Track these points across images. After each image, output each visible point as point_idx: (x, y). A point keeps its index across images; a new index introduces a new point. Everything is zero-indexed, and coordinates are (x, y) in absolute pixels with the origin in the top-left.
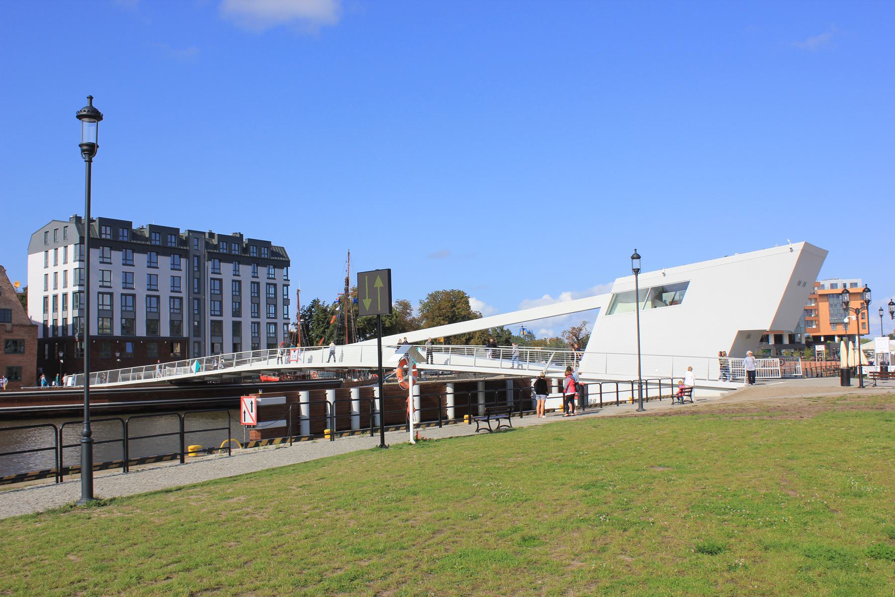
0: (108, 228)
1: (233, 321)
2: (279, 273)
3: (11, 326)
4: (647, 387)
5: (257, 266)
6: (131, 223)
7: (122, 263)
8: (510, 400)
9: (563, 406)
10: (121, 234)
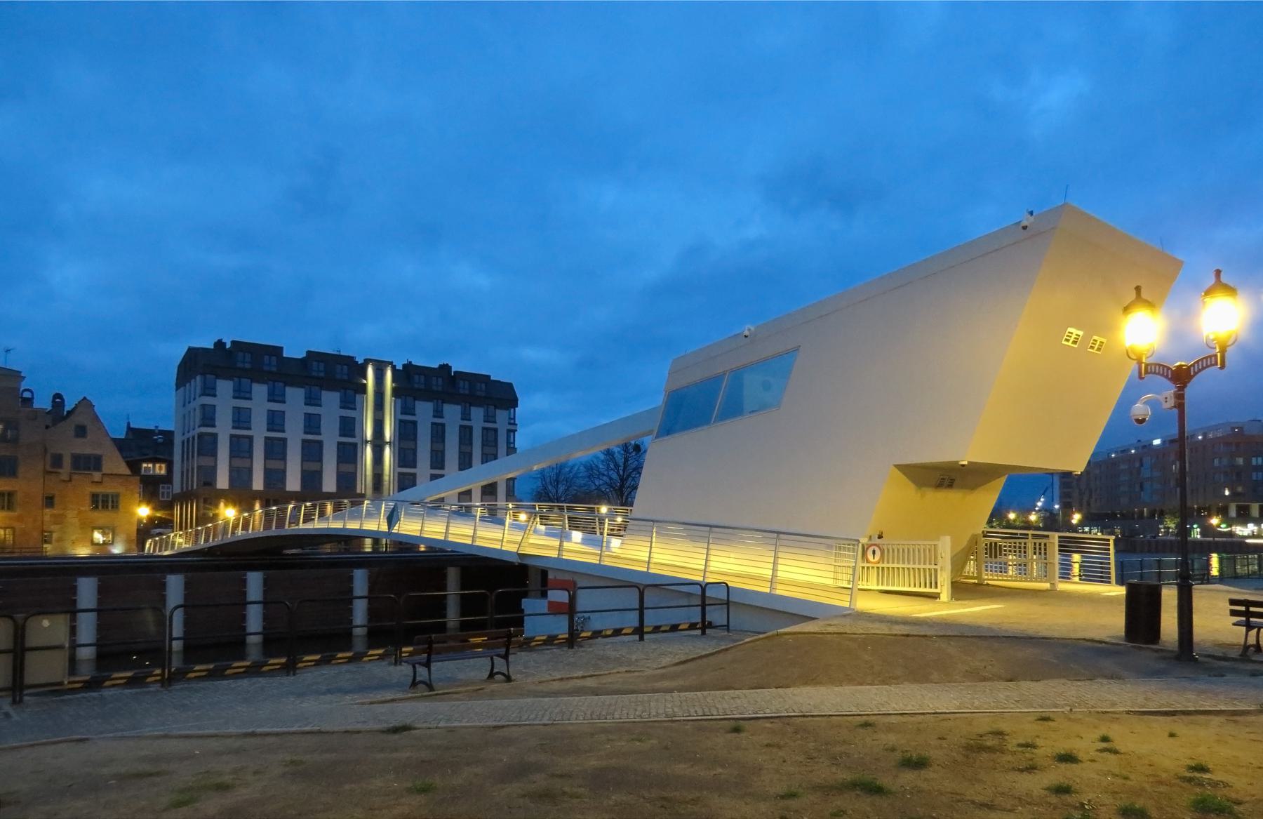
2: (501, 415)
4: (447, 529)
5: (443, 402)
7: (232, 395)
9: (1229, 656)
10: (434, 382)
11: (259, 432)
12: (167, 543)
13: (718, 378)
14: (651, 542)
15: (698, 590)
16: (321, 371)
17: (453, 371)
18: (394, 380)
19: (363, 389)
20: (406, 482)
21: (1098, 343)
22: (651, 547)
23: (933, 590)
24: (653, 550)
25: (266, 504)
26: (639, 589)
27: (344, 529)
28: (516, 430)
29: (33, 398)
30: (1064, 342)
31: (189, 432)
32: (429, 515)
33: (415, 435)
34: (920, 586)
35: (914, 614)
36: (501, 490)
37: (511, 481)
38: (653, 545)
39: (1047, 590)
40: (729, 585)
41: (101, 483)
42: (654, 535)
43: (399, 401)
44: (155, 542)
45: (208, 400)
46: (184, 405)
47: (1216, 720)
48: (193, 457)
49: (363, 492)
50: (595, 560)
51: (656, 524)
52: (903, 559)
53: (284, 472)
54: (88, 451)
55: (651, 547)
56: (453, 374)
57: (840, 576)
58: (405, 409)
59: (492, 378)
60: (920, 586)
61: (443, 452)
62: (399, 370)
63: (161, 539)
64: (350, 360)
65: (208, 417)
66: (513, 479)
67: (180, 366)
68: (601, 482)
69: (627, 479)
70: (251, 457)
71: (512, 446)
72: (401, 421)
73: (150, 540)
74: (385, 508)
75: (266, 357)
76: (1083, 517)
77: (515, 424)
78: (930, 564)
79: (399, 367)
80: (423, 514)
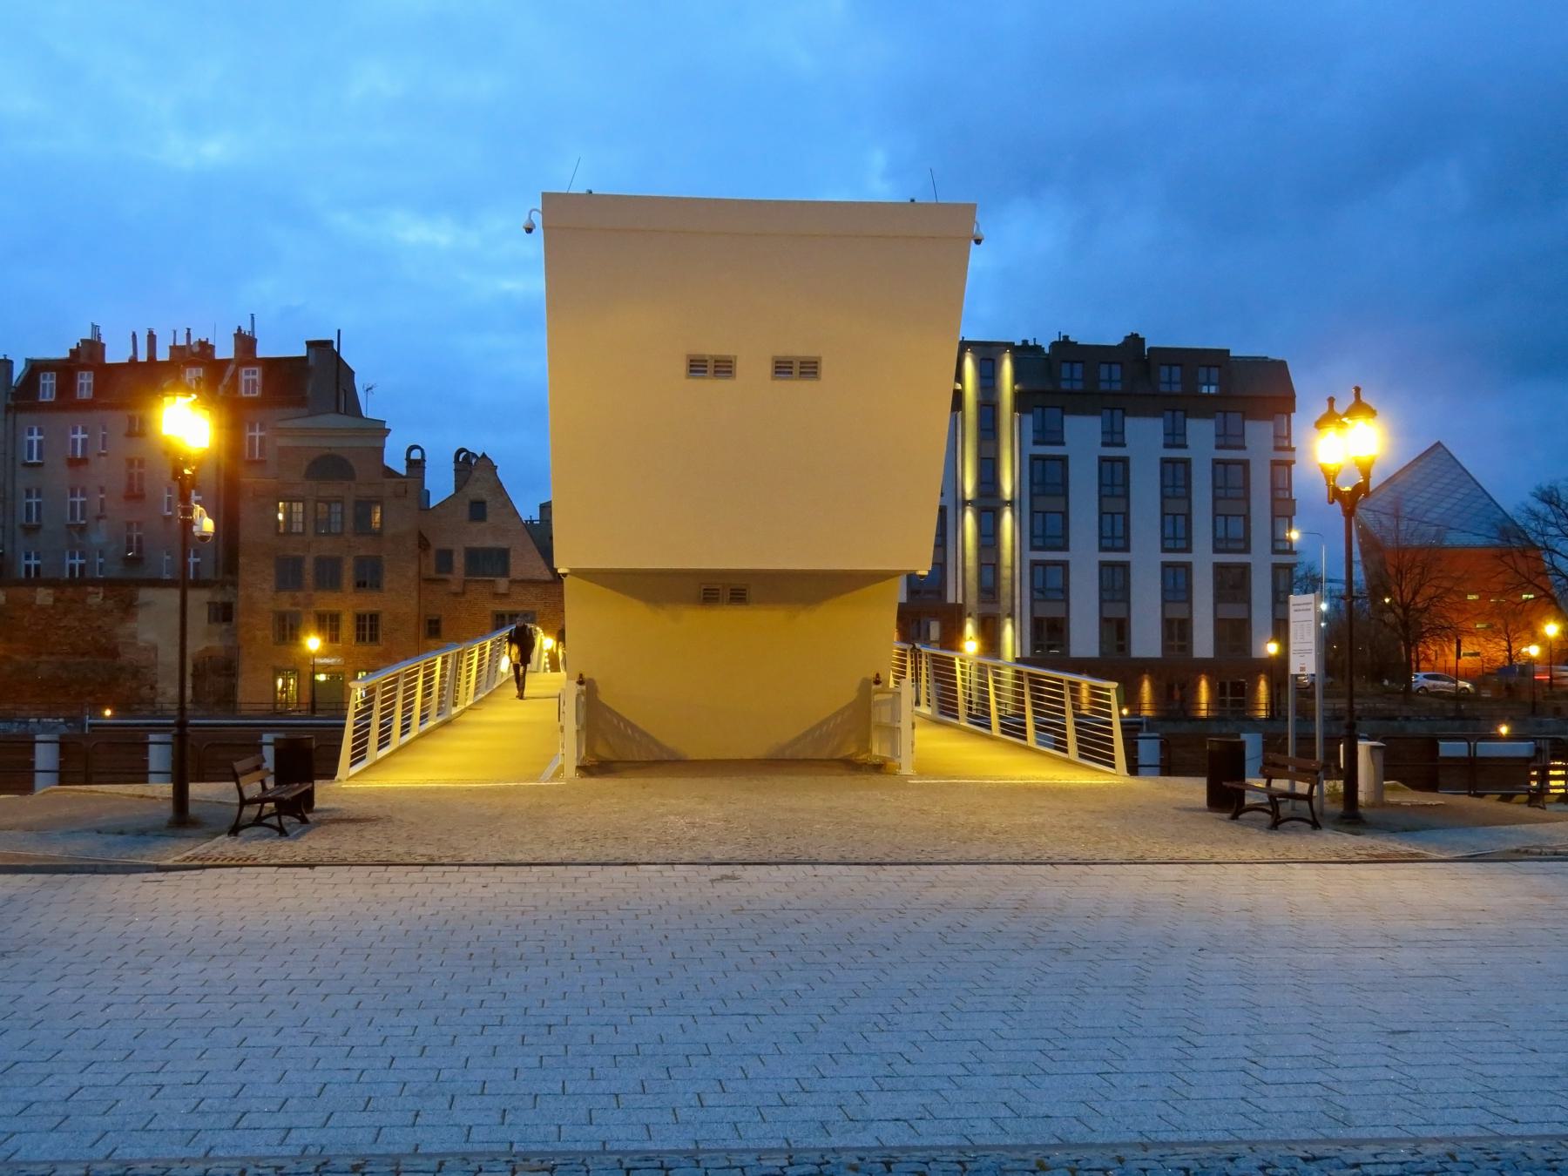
0: (1116, 369)
1: (1162, 562)
3: (507, 583)
6: (1228, 351)
8: (1272, 757)
16: (1176, 383)
17: (1146, 347)
18: (1017, 378)
28: (1294, 462)
29: (423, 460)
41: (505, 595)
43: (1029, 419)
47: (822, 861)
49: (960, 601)
52: (741, 594)
54: (489, 542)
58: (1047, 434)
59: (1079, 343)
72: (1034, 459)
75: (1066, 368)
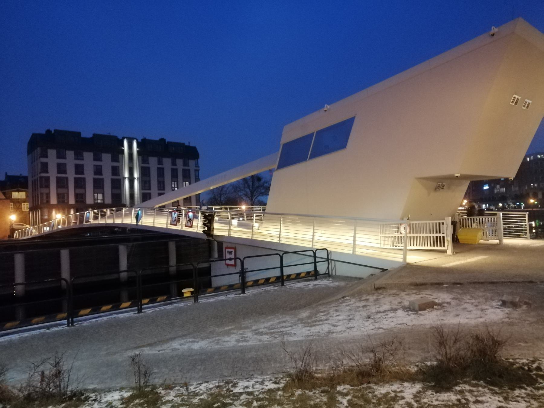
2: (192, 163)
11: (71, 175)
12: (25, 233)
13: (309, 137)
14: (280, 226)
15: (311, 253)
18: (138, 147)
19: (123, 151)
20: (145, 197)
21: (528, 103)
22: (280, 229)
23: (442, 248)
24: (282, 231)
25: (77, 211)
26: (280, 255)
27: (114, 223)
28: (199, 170)
30: (511, 103)
31: (35, 176)
32: (157, 214)
33: (149, 174)
34: (431, 246)
35: (444, 264)
36: (194, 201)
37: (198, 196)
38: (282, 228)
39: (497, 244)
40: (328, 250)
42: (282, 222)
44: (19, 232)
45: (44, 160)
46: (32, 163)
48: (38, 189)
50: (249, 236)
51: (282, 216)
53: (85, 194)
55: (280, 229)
56: (166, 143)
57: (387, 243)
60: (431, 246)
61: (163, 182)
62: (140, 142)
63: (22, 231)
64: (115, 137)
65: (45, 167)
66: (199, 194)
67: (29, 143)
68: (242, 194)
69: (254, 192)
70: (67, 188)
71: (197, 177)
73: (16, 232)
74: (134, 212)
76: (528, 202)
77: (198, 167)
78: (433, 233)
79: (140, 140)
80: (154, 215)
